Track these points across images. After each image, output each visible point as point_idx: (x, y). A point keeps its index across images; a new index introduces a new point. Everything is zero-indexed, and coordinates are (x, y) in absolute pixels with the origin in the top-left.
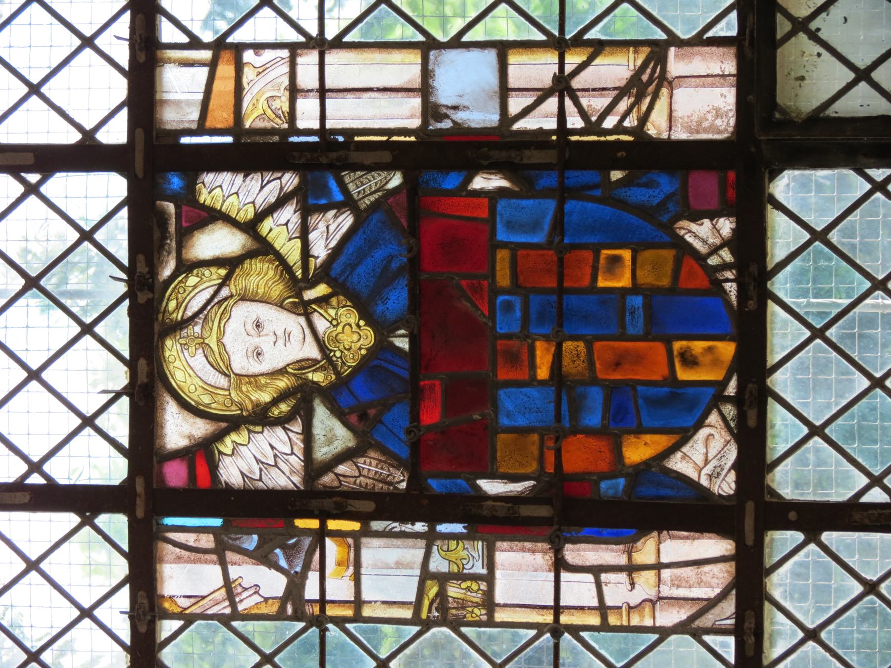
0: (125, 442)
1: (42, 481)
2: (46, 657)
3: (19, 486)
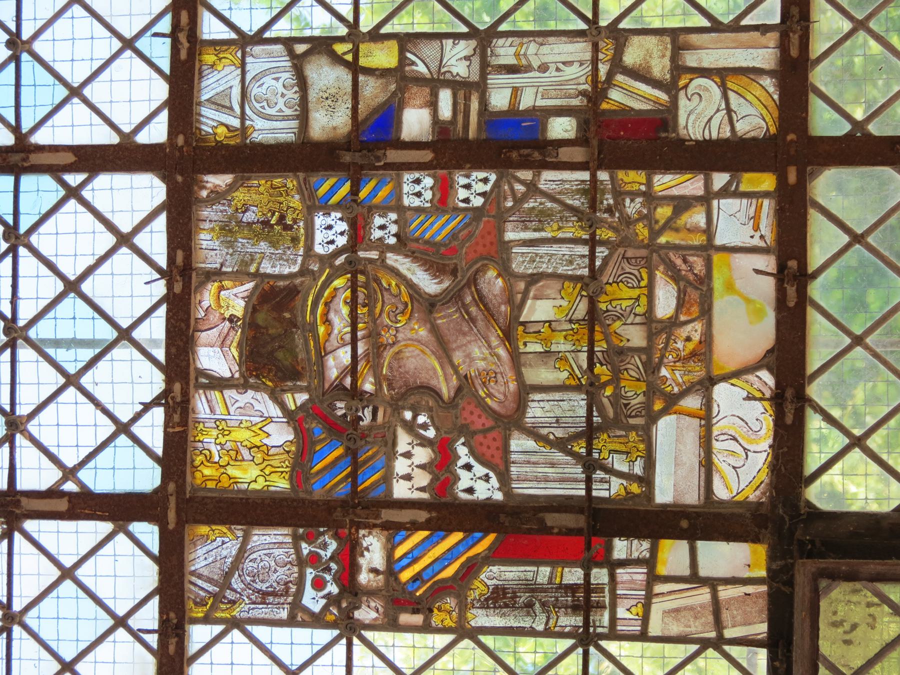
0: (159, 451)
2: (79, 667)
3: (53, 493)
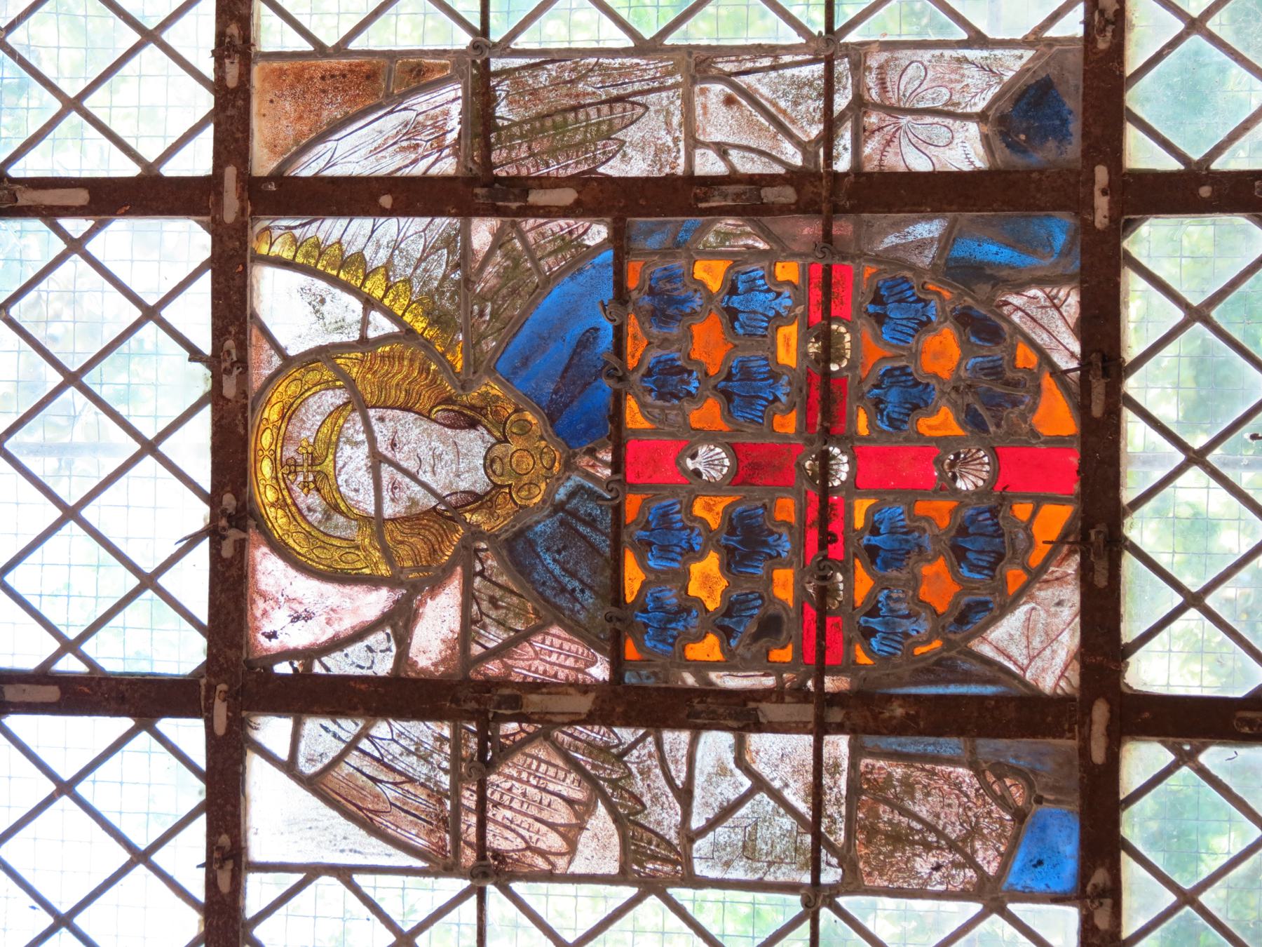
1: (80, 668)
3: (43, 676)
